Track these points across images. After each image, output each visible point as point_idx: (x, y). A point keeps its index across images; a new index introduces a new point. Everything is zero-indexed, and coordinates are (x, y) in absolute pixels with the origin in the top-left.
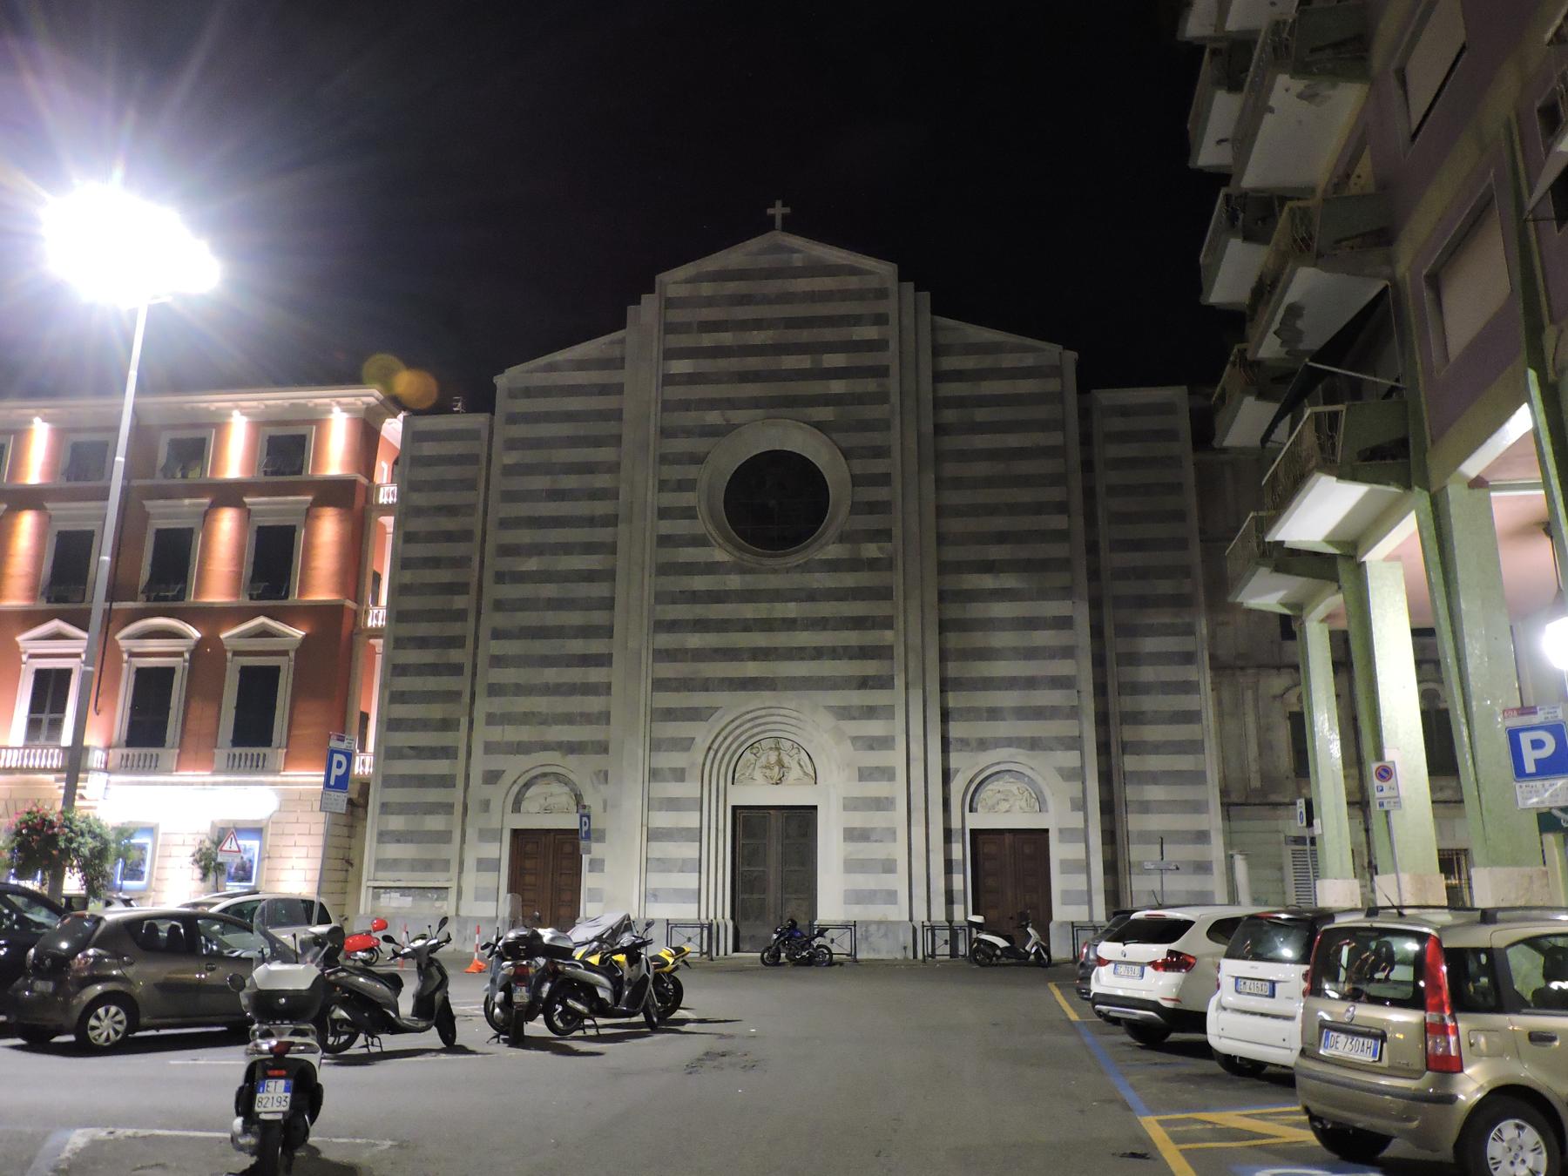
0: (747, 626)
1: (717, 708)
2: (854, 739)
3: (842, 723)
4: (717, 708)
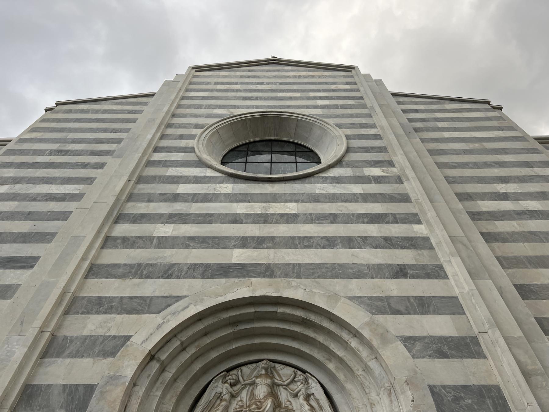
0: (236, 219)
1: (178, 298)
2: (409, 341)
3: (381, 318)
4: (178, 298)
